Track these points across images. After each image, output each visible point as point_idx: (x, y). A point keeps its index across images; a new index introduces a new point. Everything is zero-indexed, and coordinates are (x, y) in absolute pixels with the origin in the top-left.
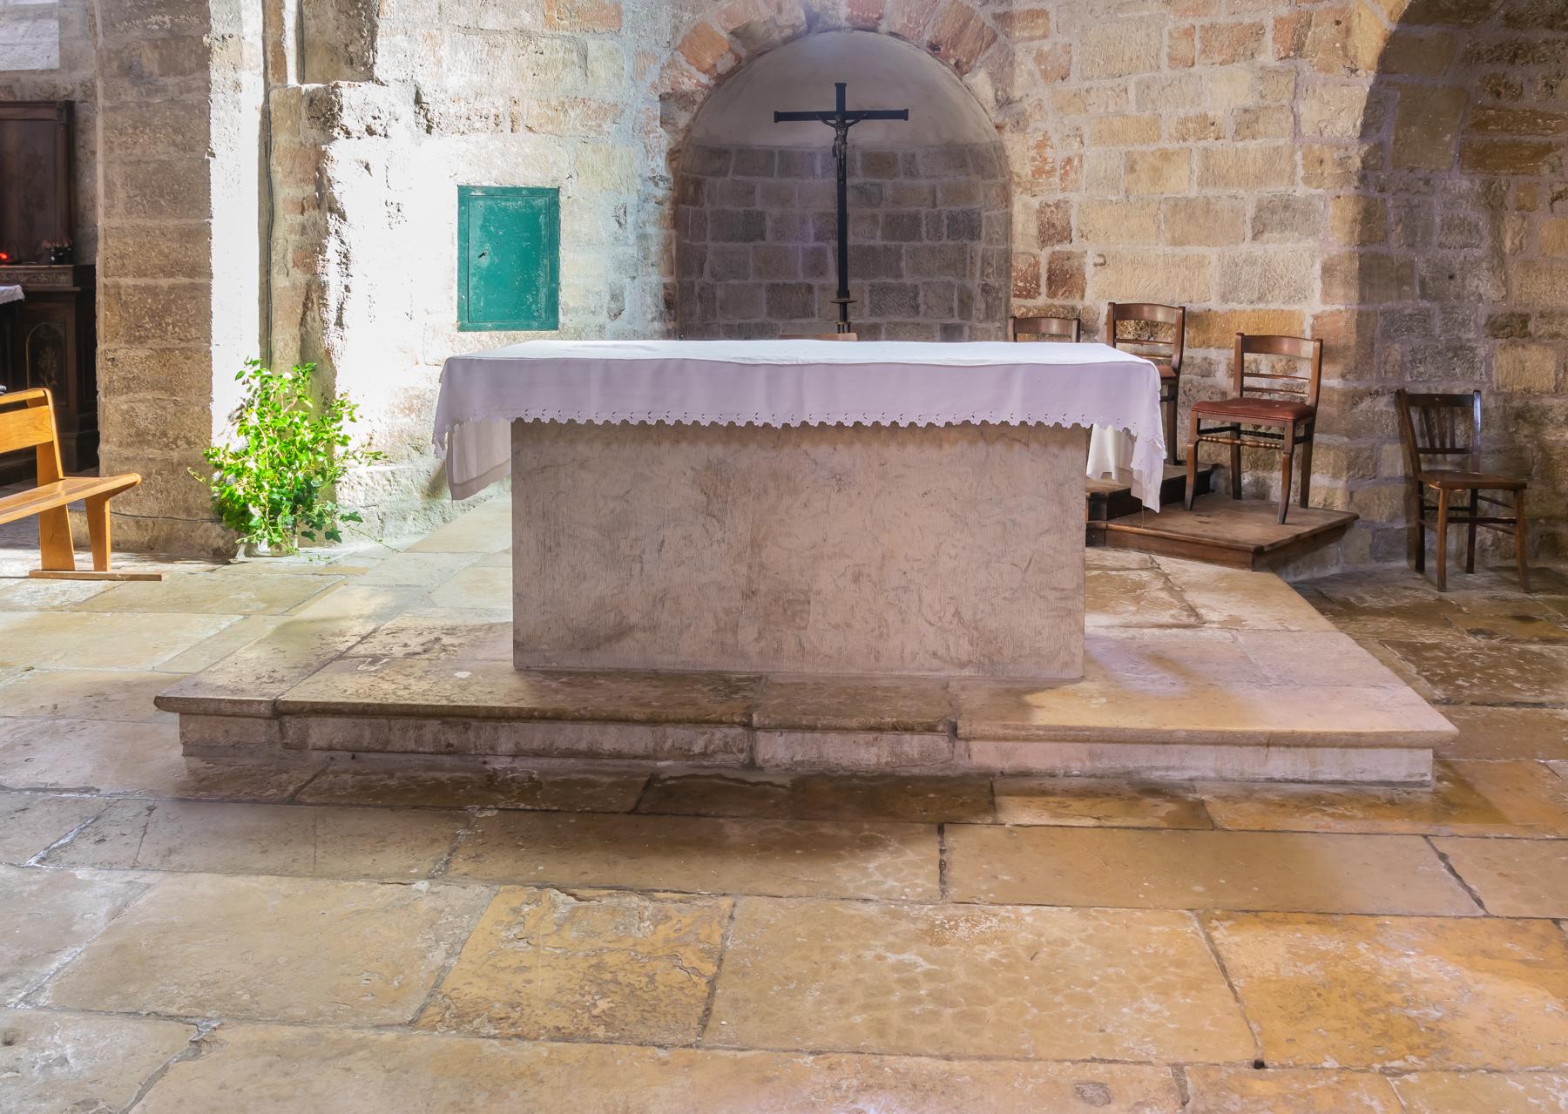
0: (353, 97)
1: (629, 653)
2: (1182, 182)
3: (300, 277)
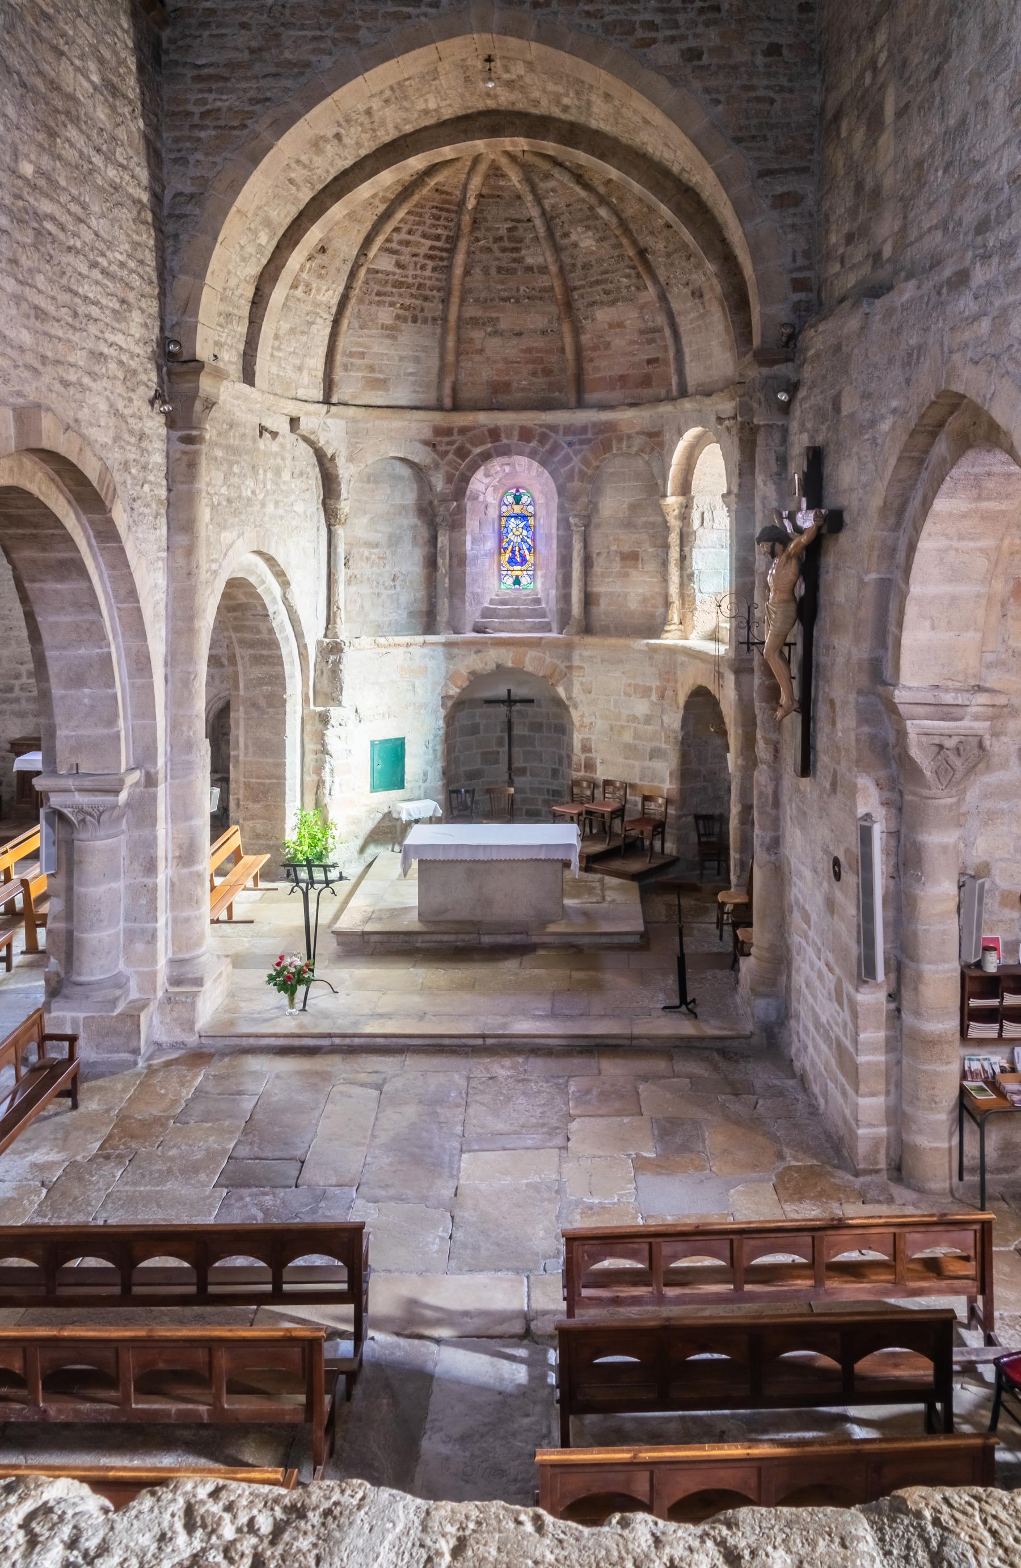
0: (334, 712)
1: (448, 916)
2: (628, 737)
3: (315, 777)
